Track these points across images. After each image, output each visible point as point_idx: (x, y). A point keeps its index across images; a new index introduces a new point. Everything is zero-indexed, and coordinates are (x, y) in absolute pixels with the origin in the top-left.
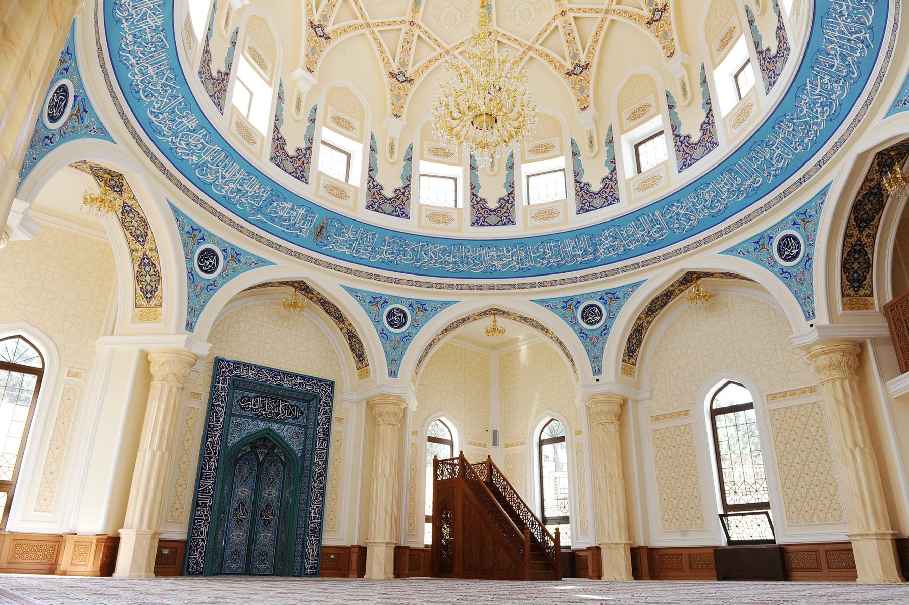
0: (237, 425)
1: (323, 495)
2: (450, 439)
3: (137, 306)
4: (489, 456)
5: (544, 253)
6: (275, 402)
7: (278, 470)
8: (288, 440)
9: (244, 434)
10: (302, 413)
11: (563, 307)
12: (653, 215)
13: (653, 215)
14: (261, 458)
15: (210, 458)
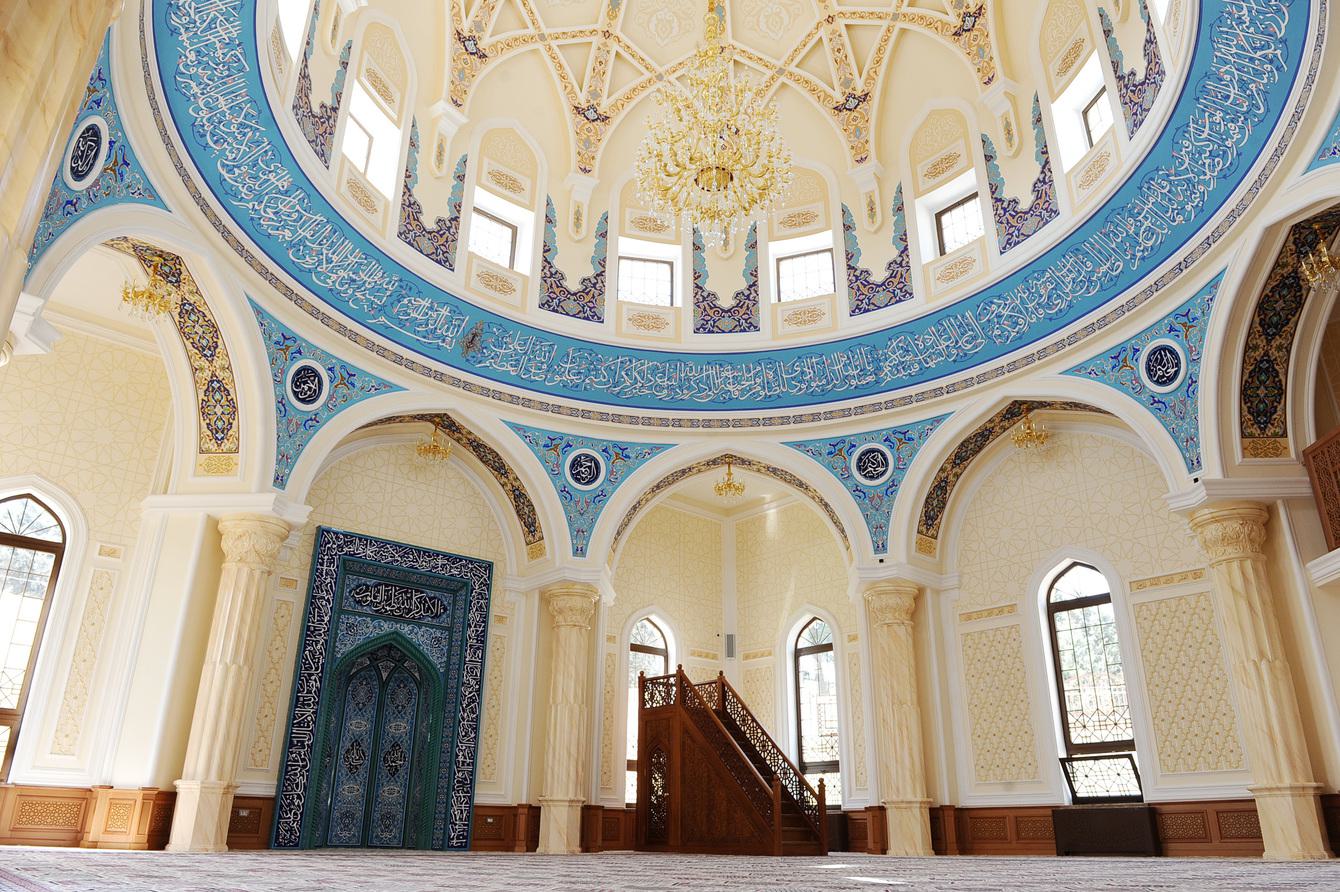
0: (350, 627)
1: (476, 729)
2: (663, 647)
4: (721, 673)
5: (803, 372)
6: (406, 593)
7: (410, 693)
8: (425, 649)
10: (445, 609)
11: (830, 453)
12: (963, 316)
13: (963, 316)
14: (385, 675)
15: (311, 675)
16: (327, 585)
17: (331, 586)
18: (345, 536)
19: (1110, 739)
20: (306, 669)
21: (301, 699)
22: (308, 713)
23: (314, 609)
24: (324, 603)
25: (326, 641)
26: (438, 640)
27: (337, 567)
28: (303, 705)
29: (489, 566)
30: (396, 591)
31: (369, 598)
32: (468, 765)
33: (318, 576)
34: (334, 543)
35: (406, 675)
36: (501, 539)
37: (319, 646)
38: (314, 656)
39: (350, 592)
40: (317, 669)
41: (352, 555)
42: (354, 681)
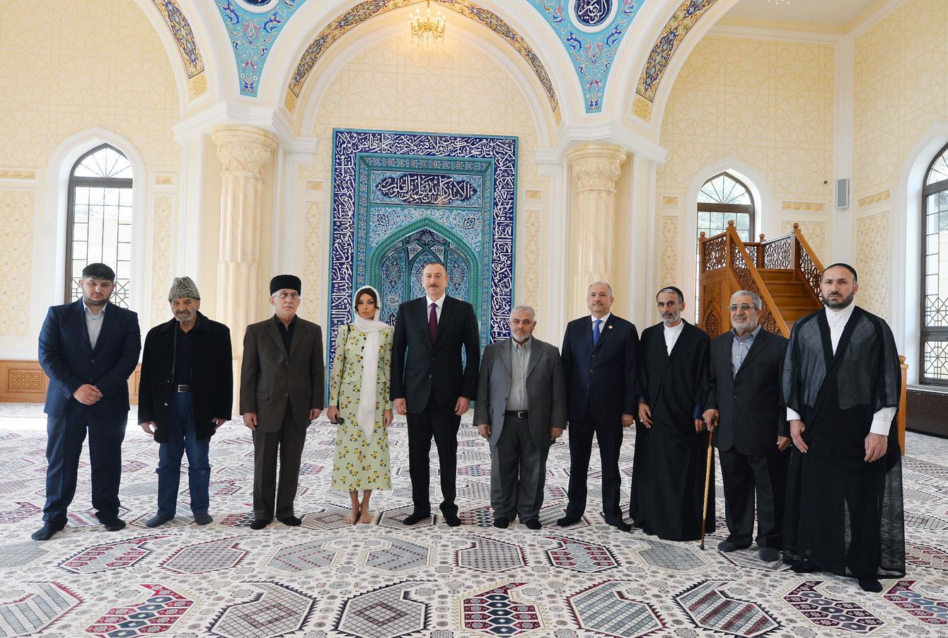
0: (381, 218)
3: (190, 77)
4: (796, 227)
6: (432, 180)
8: (459, 232)
9: (392, 229)
10: (475, 191)
14: (442, 257)
15: (342, 264)
16: (347, 183)
17: (351, 183)
18: (359, 134)
19: (77, 208)
20: (337, 259)
21: (336, 285)
22: (344, 297)
23: (338, 206)
24: (346, 199)
25: (353, 233)
26: (381, 218)
27: (355, 164)
28: (339, 290)
29: (514, 142)
30: (422, 179)
31: (395, 190)
32: (505, 335)
33: (338, 176)
34: (349, 142)
35: (456, 256)
36: (529, 111)
37: (346, 239)
38: (343, 247)
39: (377, 186)
40: (347, 258)
41: (367, 151)
42: (415, 265)
